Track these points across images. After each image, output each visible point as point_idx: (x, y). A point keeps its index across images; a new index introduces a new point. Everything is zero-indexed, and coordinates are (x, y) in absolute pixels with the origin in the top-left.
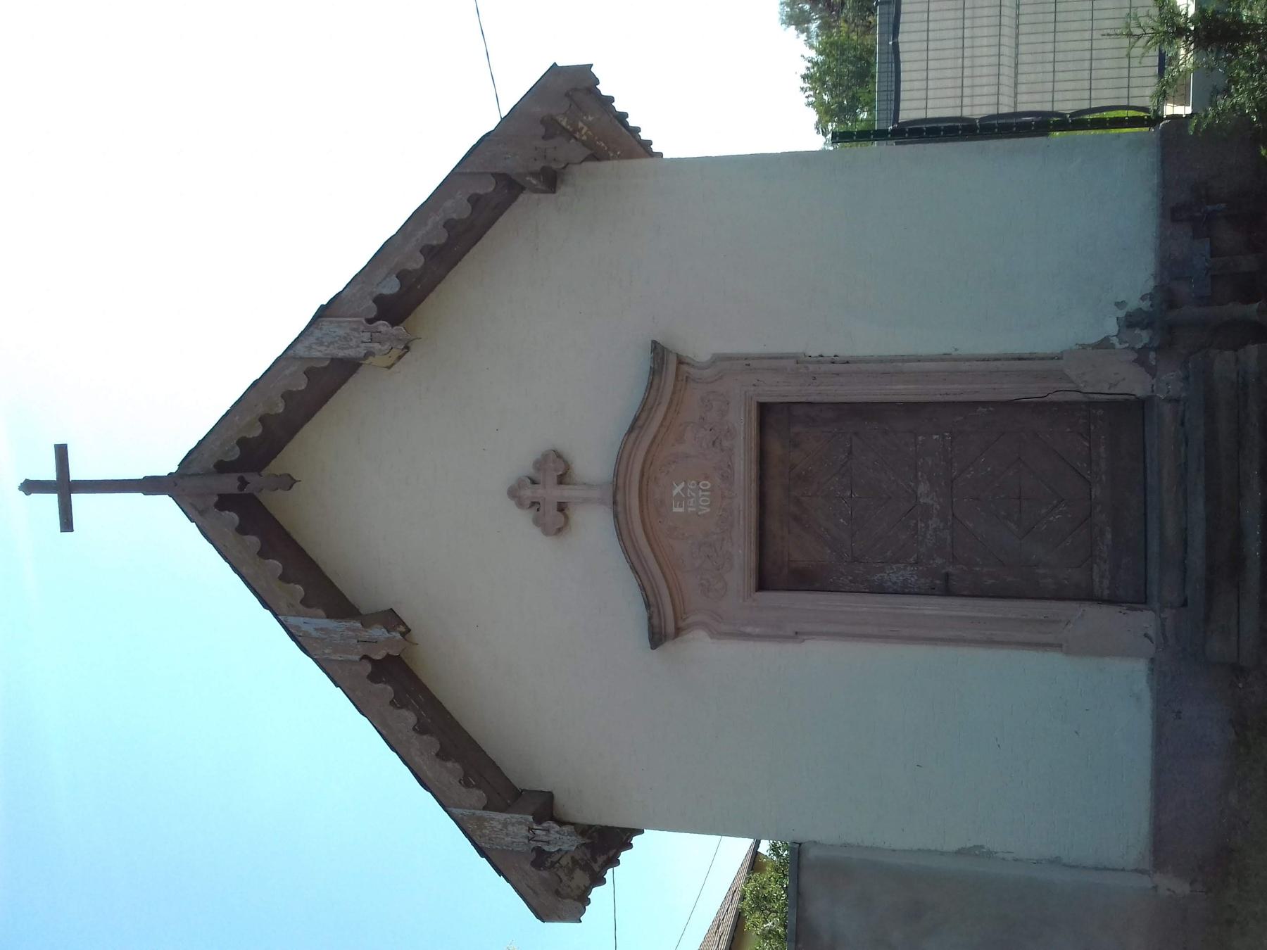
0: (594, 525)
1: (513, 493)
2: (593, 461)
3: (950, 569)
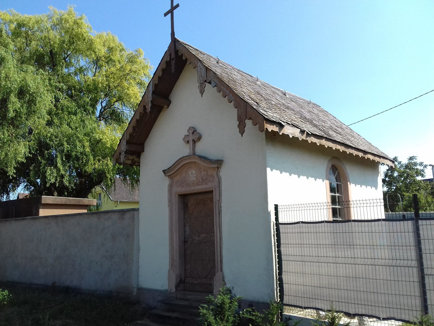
0: (186, 150)
2: (201, 148)
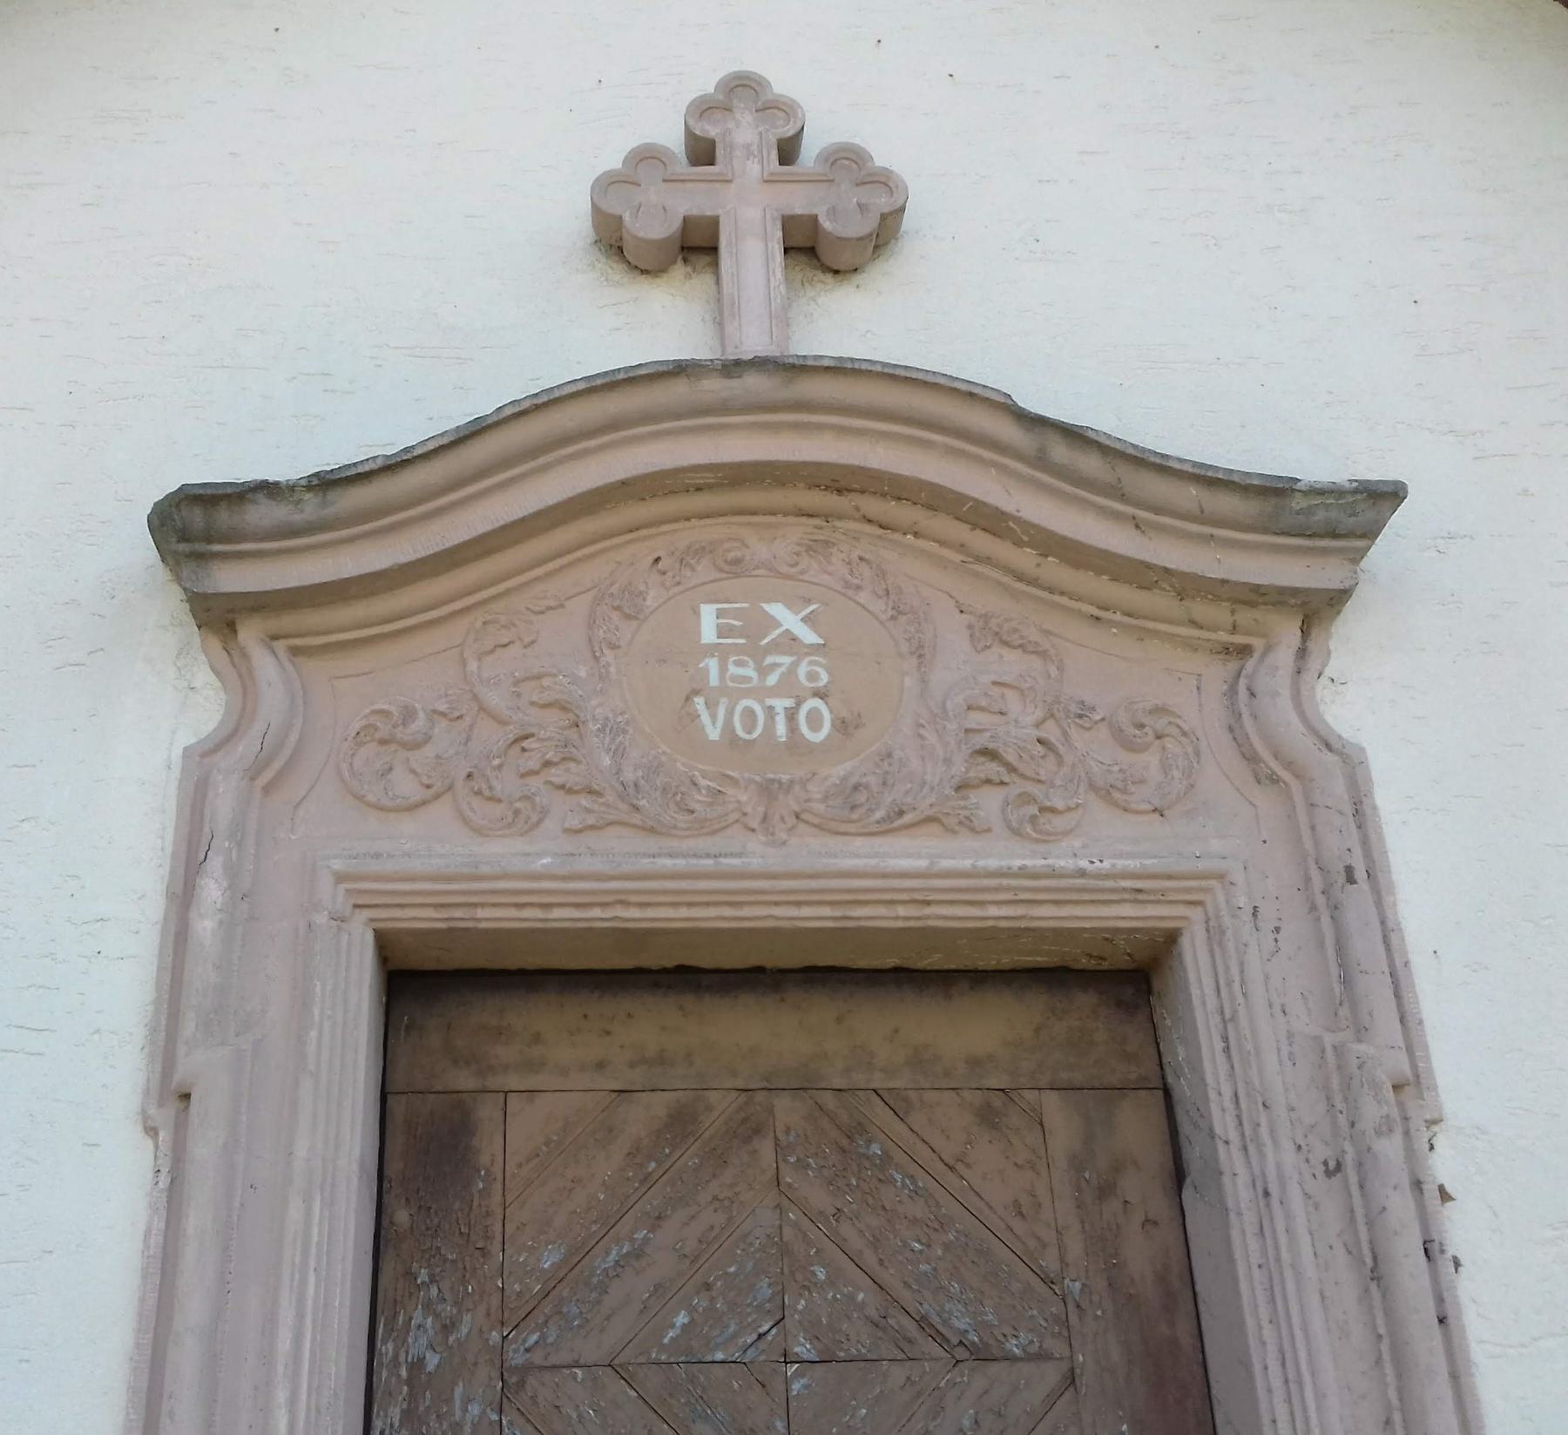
1: (743, 88)
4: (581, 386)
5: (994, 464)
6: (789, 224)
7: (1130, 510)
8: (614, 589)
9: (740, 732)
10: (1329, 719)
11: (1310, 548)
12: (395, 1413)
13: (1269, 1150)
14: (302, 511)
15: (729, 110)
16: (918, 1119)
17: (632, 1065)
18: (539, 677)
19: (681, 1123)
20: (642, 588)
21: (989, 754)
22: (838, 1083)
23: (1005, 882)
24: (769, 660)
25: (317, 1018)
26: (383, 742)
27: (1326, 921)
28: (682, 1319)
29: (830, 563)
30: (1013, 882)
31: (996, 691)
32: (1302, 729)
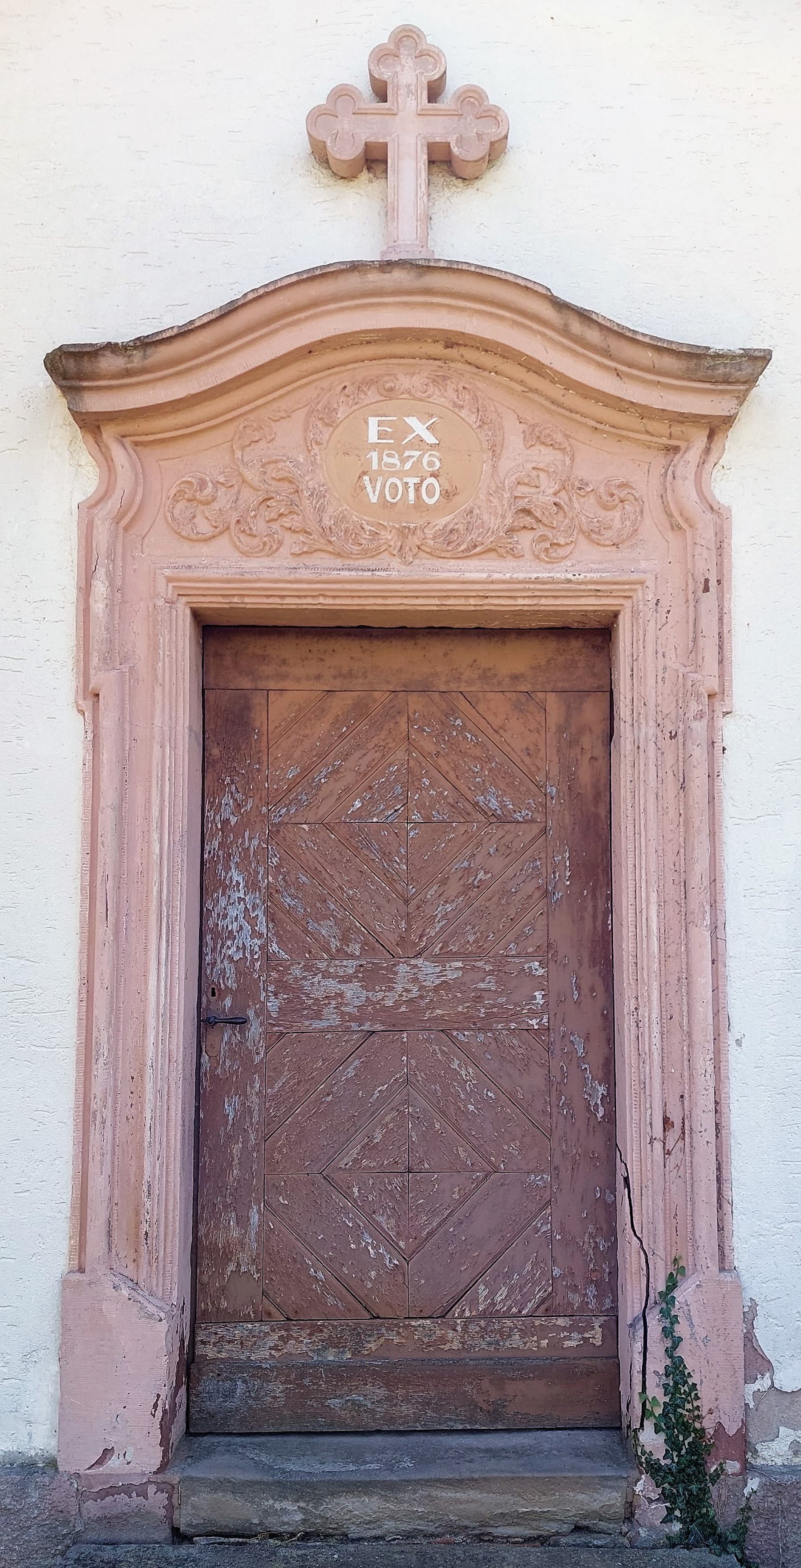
1: (406, 38)
3: (255, 1029)
4: (294, 279)
5: (539, 333)
6: (432, 148)
7: (613, 364)
8: (319, 407)
9: (388, 498)
10: (716, 492)
11: (714, 390)
12: (216, 844)
13: (643, 726)
14: (133, 362)
15: (398, 57)
16: (481, 707)
17: (335, 677)
18: (276, 462)
19: (360, 709)
20: (335, 406)
21: (527, 512)
22: (443, 688)
23: (527, 586)
24: (407, 454)
25: (161, 656)
26: (189, 500)
27: (691, 608)
28: (358, 804)
29: (445, 390)
30: (532, 586)
31: (534, 473)
32: (696, 499)
